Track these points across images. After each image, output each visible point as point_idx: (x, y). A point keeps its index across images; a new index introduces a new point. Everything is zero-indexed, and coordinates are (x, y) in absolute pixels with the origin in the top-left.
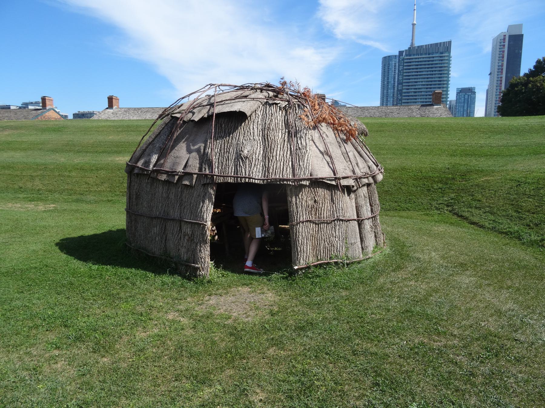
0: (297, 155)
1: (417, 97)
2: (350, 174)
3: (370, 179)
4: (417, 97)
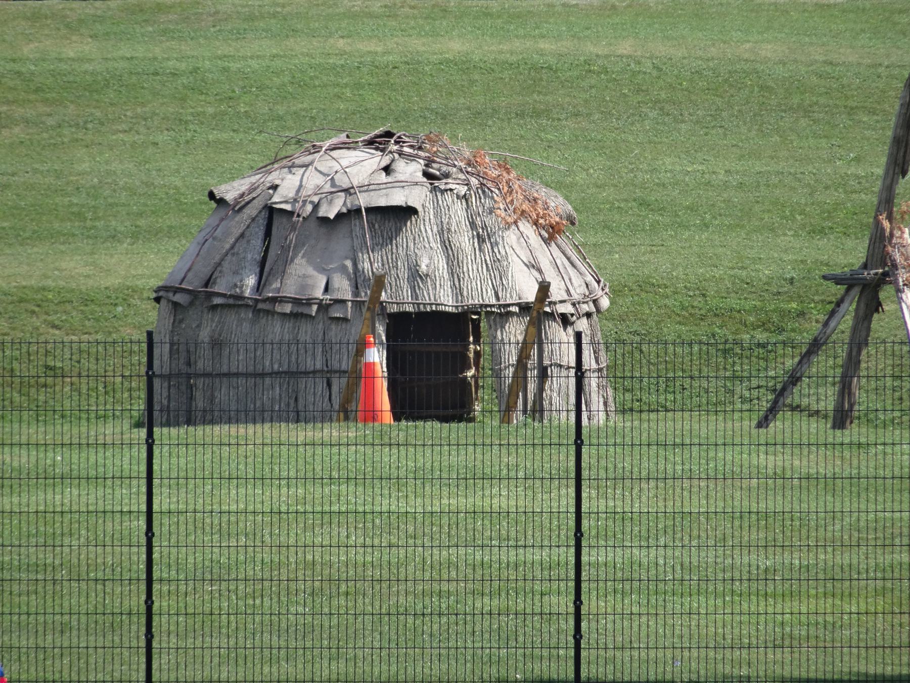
0: (497, 268)
2: (566, 297)
3: (591, 304)
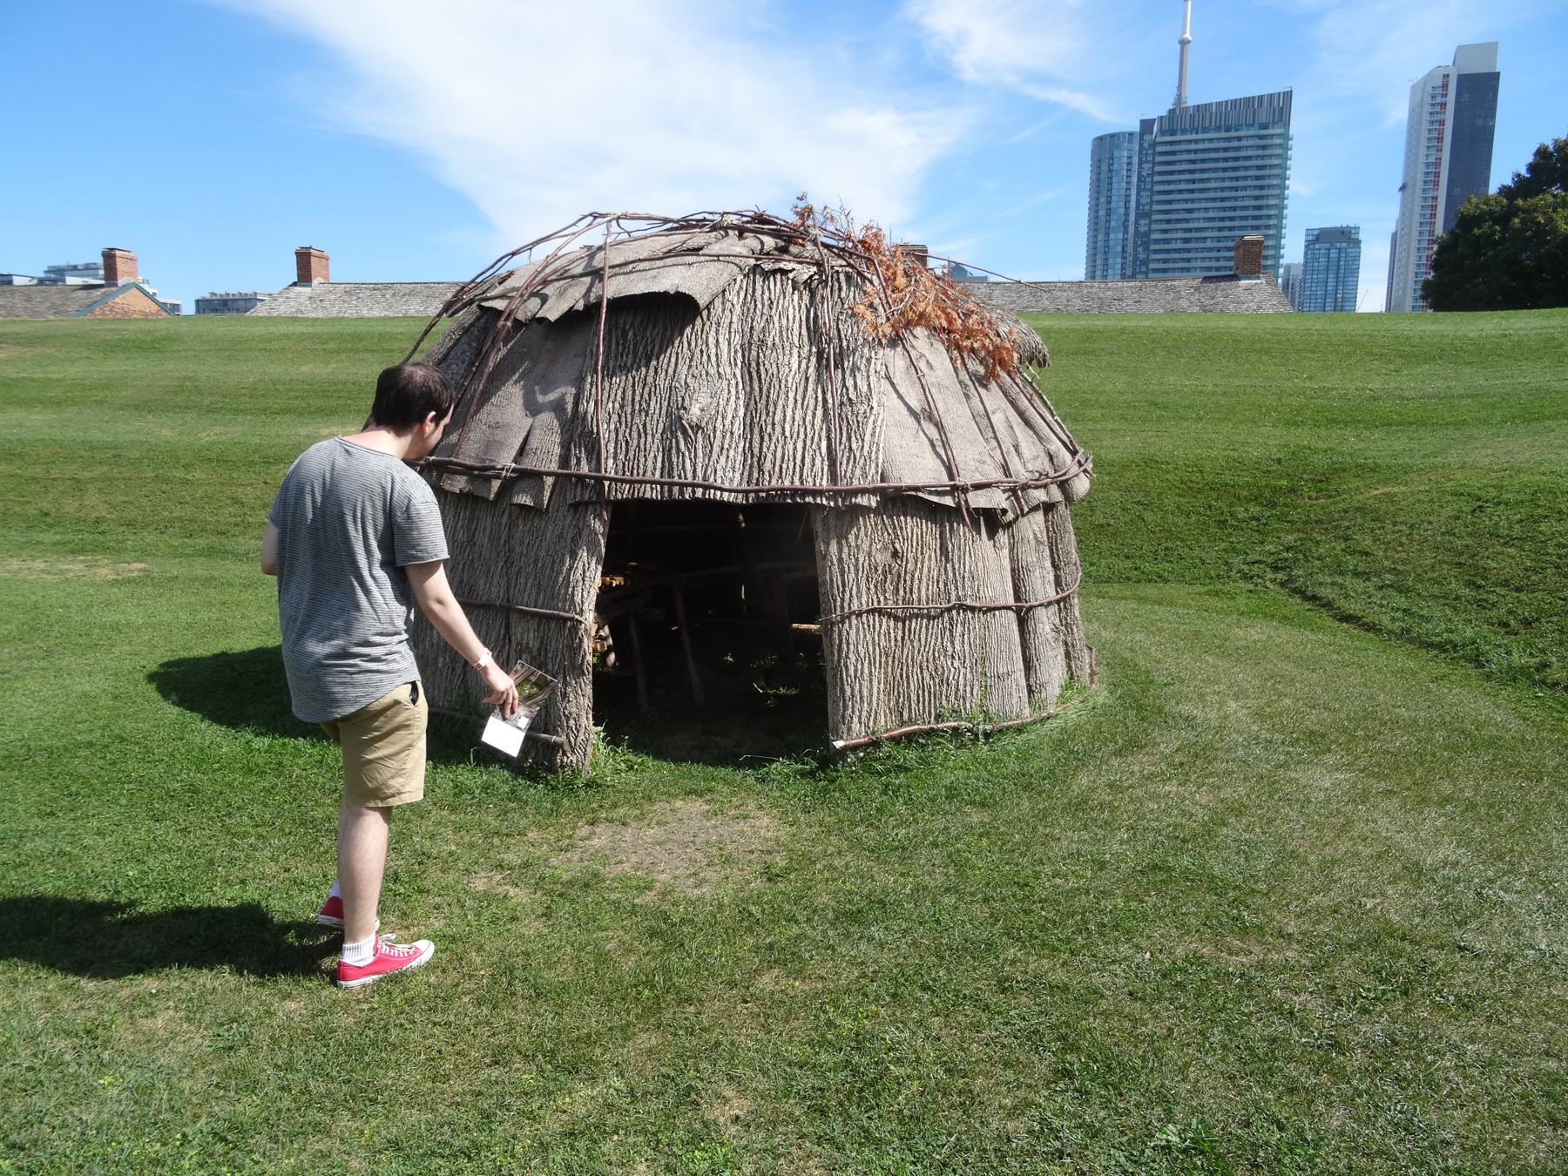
0: (842, 420)
1: (1192, 255)
3: (1055, 490)
4: (1192, 255)
